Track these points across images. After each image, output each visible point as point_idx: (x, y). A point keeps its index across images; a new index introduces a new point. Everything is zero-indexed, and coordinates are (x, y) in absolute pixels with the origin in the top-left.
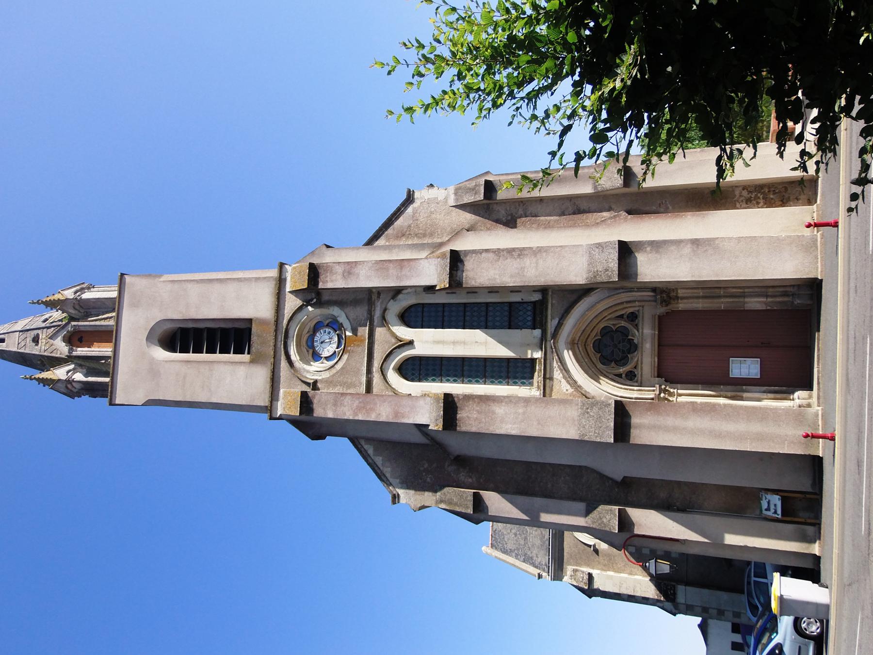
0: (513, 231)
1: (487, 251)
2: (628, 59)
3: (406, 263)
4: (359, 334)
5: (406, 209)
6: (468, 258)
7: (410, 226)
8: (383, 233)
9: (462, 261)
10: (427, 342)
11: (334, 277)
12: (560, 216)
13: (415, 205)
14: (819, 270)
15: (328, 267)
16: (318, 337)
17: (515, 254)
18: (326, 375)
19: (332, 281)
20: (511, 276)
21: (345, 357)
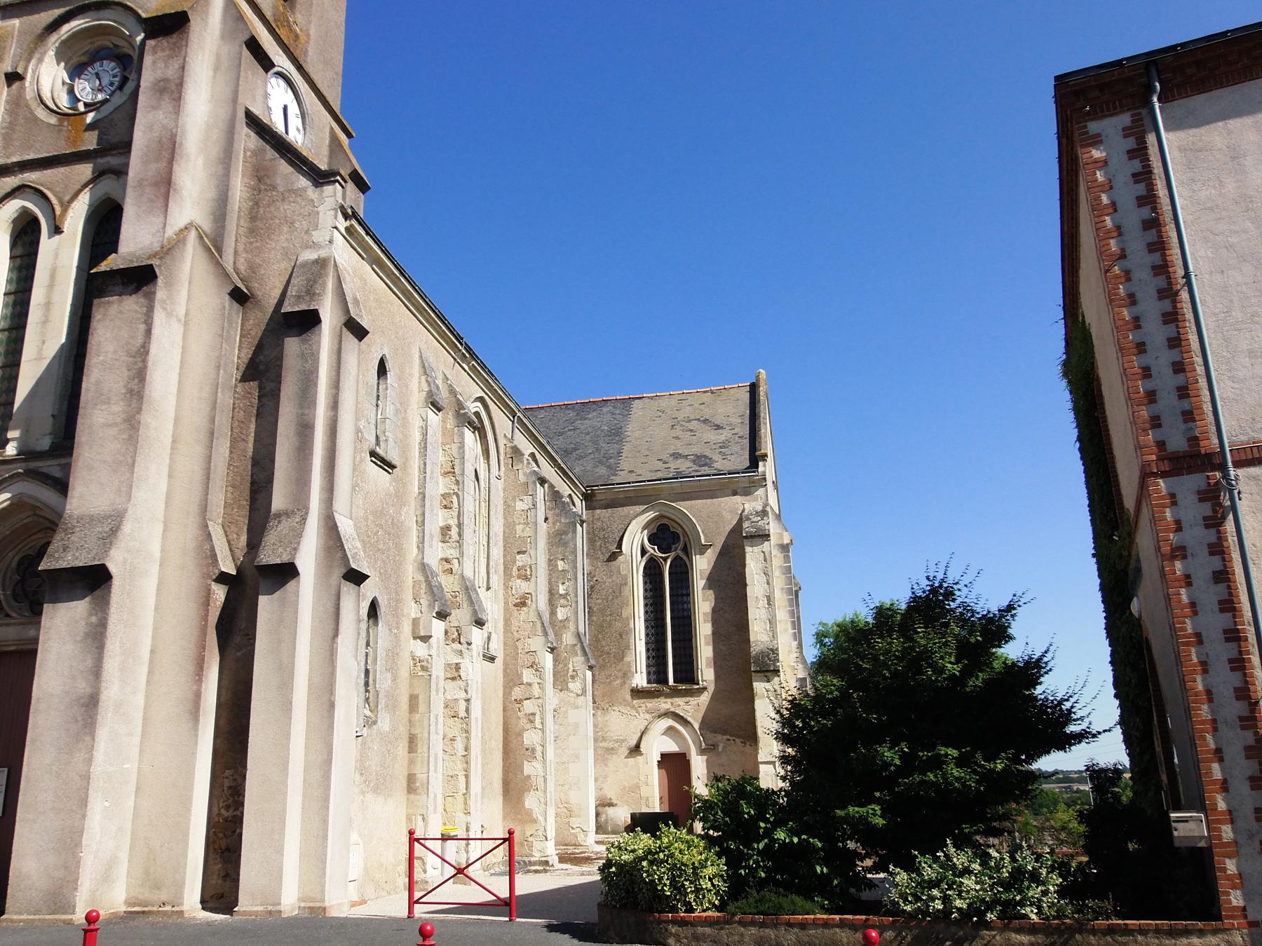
0: (236, 375)
1: (149, 332)
3: (163, 190)
4: (87, 134)
5: (305, 174)
6: (142, 300)
7: (274, 188)
8: (267, 142)
9: (136, 290)
10: (56, 256)
11: (160, 64)
13: (312, 192)
14: (15, 917)
15: (179, 52)
16: (109, 65)
17: (134, 385)
18: (29, 94)
19: (154, 62)
20: (98, 382)
21: (53, 120)
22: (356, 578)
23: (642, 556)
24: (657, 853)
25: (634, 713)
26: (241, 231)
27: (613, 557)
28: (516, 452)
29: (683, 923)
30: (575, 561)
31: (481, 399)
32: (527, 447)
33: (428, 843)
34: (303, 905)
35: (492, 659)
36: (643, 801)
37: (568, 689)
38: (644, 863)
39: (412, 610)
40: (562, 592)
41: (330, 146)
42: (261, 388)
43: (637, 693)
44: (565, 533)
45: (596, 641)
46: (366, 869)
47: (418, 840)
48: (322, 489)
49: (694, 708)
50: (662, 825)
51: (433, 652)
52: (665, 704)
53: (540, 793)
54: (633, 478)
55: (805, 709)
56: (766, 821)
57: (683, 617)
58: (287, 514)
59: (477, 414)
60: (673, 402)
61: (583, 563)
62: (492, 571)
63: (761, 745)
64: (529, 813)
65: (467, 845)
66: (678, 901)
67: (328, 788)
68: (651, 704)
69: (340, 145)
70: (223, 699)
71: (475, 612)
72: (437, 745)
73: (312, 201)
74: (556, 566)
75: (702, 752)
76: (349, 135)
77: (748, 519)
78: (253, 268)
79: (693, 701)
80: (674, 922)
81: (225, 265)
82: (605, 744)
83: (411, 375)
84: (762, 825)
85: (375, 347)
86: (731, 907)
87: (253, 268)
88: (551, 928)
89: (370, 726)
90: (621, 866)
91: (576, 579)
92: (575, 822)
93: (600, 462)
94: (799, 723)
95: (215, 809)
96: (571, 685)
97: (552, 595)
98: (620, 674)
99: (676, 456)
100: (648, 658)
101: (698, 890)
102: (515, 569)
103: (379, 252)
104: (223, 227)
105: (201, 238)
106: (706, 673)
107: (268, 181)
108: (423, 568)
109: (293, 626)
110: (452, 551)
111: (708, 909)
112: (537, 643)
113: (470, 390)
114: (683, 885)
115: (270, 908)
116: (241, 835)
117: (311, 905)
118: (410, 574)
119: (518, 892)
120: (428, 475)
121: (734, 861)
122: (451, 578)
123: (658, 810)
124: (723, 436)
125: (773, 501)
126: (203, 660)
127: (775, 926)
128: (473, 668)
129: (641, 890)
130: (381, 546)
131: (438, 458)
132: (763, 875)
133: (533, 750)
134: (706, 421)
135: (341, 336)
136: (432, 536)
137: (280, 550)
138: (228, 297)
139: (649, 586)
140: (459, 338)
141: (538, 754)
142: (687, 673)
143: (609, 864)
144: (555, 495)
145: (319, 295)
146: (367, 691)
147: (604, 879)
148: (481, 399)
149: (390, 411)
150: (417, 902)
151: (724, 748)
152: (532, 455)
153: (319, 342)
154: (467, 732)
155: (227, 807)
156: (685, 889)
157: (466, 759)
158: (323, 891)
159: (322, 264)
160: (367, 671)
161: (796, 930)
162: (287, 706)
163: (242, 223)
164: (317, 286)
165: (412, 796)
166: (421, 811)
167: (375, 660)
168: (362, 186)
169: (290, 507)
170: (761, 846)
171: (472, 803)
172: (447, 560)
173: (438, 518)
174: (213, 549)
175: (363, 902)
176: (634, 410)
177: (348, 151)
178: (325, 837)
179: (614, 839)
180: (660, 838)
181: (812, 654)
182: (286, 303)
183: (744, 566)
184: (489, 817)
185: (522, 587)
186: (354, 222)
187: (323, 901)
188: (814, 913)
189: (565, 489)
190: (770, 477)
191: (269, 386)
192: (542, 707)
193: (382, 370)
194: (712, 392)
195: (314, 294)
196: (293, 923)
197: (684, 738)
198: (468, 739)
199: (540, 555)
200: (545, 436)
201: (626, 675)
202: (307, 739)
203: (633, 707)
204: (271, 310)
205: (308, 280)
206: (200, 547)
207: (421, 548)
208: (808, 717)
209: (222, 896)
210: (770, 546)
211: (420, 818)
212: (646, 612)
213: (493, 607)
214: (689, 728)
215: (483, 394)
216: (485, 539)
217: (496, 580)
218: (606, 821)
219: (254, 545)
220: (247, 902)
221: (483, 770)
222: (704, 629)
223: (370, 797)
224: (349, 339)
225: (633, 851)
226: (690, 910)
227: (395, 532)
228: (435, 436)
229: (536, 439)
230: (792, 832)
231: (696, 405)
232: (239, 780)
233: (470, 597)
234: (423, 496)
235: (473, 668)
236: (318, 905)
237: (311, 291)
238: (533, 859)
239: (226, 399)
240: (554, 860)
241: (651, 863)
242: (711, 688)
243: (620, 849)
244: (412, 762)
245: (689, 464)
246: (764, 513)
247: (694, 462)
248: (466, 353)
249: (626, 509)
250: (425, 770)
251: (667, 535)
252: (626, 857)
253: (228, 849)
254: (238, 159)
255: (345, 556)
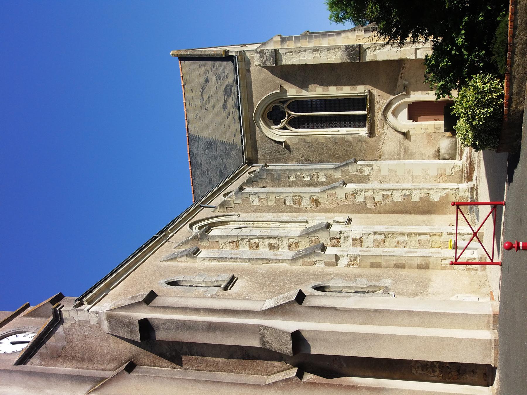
0: (178, 369)
2: (410, 35)
5: (55, 329)
7: (64, 348)
12: (228, 358)
13: (67, 325)
22: (301, 297)
23: (287, 129)
24: (468, 115)
25: (383, 136)
26: (90, 366)
27: (287, 147)
28: (223, 205)
29: (510, 101)
30: (290, 170)
31: (191, 226)
32: (220, 199)
33: (457, 257)
34: (491, 327)
35: (350, 220)
36: (437, 131)
37: (368, 175)
38: (474, 123)
39: (320, 266)
40: (309, 179)
41: (35, 317)
42: (186, 354)
43: (371, 133)
44: (273, 176)
45: (339, 159)
46: (473, 292)
47: (456, 259)
48: (247, 317)
49: (381, 98)
50: (452, 113)
51: (345, 253)
52: (378, 117)
53: (431, 192)
54: (238, 134)
55: (386, 26)
56: (451, 50)
57: (325, 105)
58: (262, 338)
59: (200, 228)
60: (191, 109)
61: (291, 166)
62: (296, 220)
63: (404, 57)
64: (442, 198)
65: (460, 234)
66: (497, 103)
67: (424, 313)
68: (378, 125)
69: (34, 311)
70: (370, 374)
71: (322, 229)
72: (401, 251)
73: (72, 324)
74: (293, 181)
75: (408, 94)
76: (28, 306)
77: (265, 63)
78: (113, 360)
79: (377, 99)
80: (509, 106)
81: (111, 376)
82: (402, 154)
83: (177, 267)
84: (453, 52)
85: (160, 287)
86: (501, 72)
87: (113, 360)
88: (510, 180)
89: (389, 290)
90: (475, 138)
91: (301, 169)
92: (448, 172)
93: (228, 154)
94: (394, 30)
95: (435, 378)
96: (366, 173)
97: (310, 184)
98: (360, 144)
99: (225, 107)
100: (350, 126)
101: (491, 91)
102: (295, 206)
103: (102, 285)
104: (88, 377)
105: (95, 390)
106: (360, 90)
107: (60, 351)
108: (294, 259)
109: (328, 335)
110: (284, 242)
111: (502, 86)
112: (340, 193)
113: (185, 232)
114: (487, 100)
115: (493, 346)
116: (450, 363)
117: (492, 323)
118: (298, 267)
119: (488, 200)
120: (238, 256)
121: (474, 70)
122: (301, 243)
123: (443, 122)
124: (212, 78)
125: (254, 47)
126: (348, 386)
127: (514, 45)
128: (356, 230)
129: (489, 126)
130: (281, 284)
131: (227, 251)
132: (483, 52)
133: (405, 196)
134: (203, 89)
135: (155, 307)
136: (275, 255)
137: (284, 341)
138: (131, 374)
139: (306, 125)
140: (154, 238)
141: (407, 193)
142: (359, 102)
143: (474, 146)
144: (249, 182)
145: (130, 319)
146: (368, 292)
147: (483, 149)
148: (191, 226)
149: (199, 279)
150: (492, 260)
151: (406, 80)
152: (225, 195)
153: (159, 319)
154: (393, 234)
155: (434, 371)
156: (490, 99)
157: (409, 234)
158: (484, 316)
159: (110, 318)
160: (356, 292)
161: (517, 32)
162: (376, 337)
163: (85, 366)
164: (124, 321)
165: (431, 266)
166: (439, 262)
167: (350, 287)
168: (60, 297)
169: (258, 336)
170: (465, 53)
171: (435, 231)
172: (290, 246)
173: (264, 251)
174: (283, 381)
175: (491, 294)
176: (196, 134)
177: (38, 306)
178: (453, 314)
179: (459, 141)
180: (460, 114)
181: (349, 24)
182: (135, 339)
183: (294, 66)
184: (444, 223)
185: (306, 202)
186: (85, 299)
187: (490, 315)
188: (507, 21)
189: (245, 176)
190: (238, 48)
191: (185, 349)
192: (379, 190)
193: (174, 283)
194: (185, 84)
195: (129, 322)
196: (502, 332)
197: (399, 105)
198: (397, 233)
199: (285, 190)
200: (212, 188)
201: (360, 140)
202: (396, 325)
203: (380, 136)
204: (139, 348)
205: (121, 326)
206: (281, 388)
207: (283, 261)
208: (391, 24)
209: (485, 374)
210: (282, 49)
211: (443, 262)
212: (322, 127)
213: (318, 219)
214: (393, 101)
215: (188, 225)
216: (276, 224)
217: (302, 217)
218: (448, 154)
219: (279, 357)
220: (490, 360)
221: (417, 225)
222: (333, 91)
223: (430, 291)
224: (157, 302)
225: (467, 131)
226: (502, 96)
227: (273, 276)
228: (214, 253)
229: (215, 193)
230: (458, 34)
231: (193, 94)
232: (419, 364)
233: (312, 232)
234: (251, 260)
235: (356, 230)
236: (492, 319)
237: (128, 324)
238: (469, 196)
239: (193, 374)
240: (470, 184)
241: (474, 119)
242: (369, 87)
243: (465, 139)
244: (411, 267)
245: (230, 99)
246: (261, 53)
247: (228, 96)
248: (162, 234)
249: (258, 139)
250: (415, 259)
251: (274, 113)
252: (470, 135)
253: (458, 371)
254: (47, 369)
255: (288, 303)
